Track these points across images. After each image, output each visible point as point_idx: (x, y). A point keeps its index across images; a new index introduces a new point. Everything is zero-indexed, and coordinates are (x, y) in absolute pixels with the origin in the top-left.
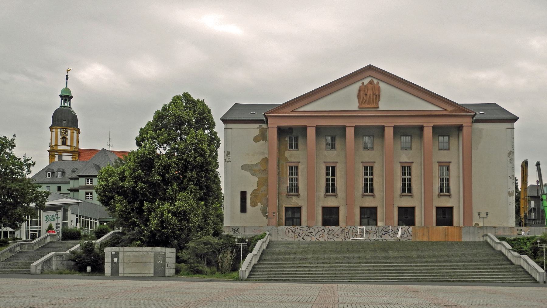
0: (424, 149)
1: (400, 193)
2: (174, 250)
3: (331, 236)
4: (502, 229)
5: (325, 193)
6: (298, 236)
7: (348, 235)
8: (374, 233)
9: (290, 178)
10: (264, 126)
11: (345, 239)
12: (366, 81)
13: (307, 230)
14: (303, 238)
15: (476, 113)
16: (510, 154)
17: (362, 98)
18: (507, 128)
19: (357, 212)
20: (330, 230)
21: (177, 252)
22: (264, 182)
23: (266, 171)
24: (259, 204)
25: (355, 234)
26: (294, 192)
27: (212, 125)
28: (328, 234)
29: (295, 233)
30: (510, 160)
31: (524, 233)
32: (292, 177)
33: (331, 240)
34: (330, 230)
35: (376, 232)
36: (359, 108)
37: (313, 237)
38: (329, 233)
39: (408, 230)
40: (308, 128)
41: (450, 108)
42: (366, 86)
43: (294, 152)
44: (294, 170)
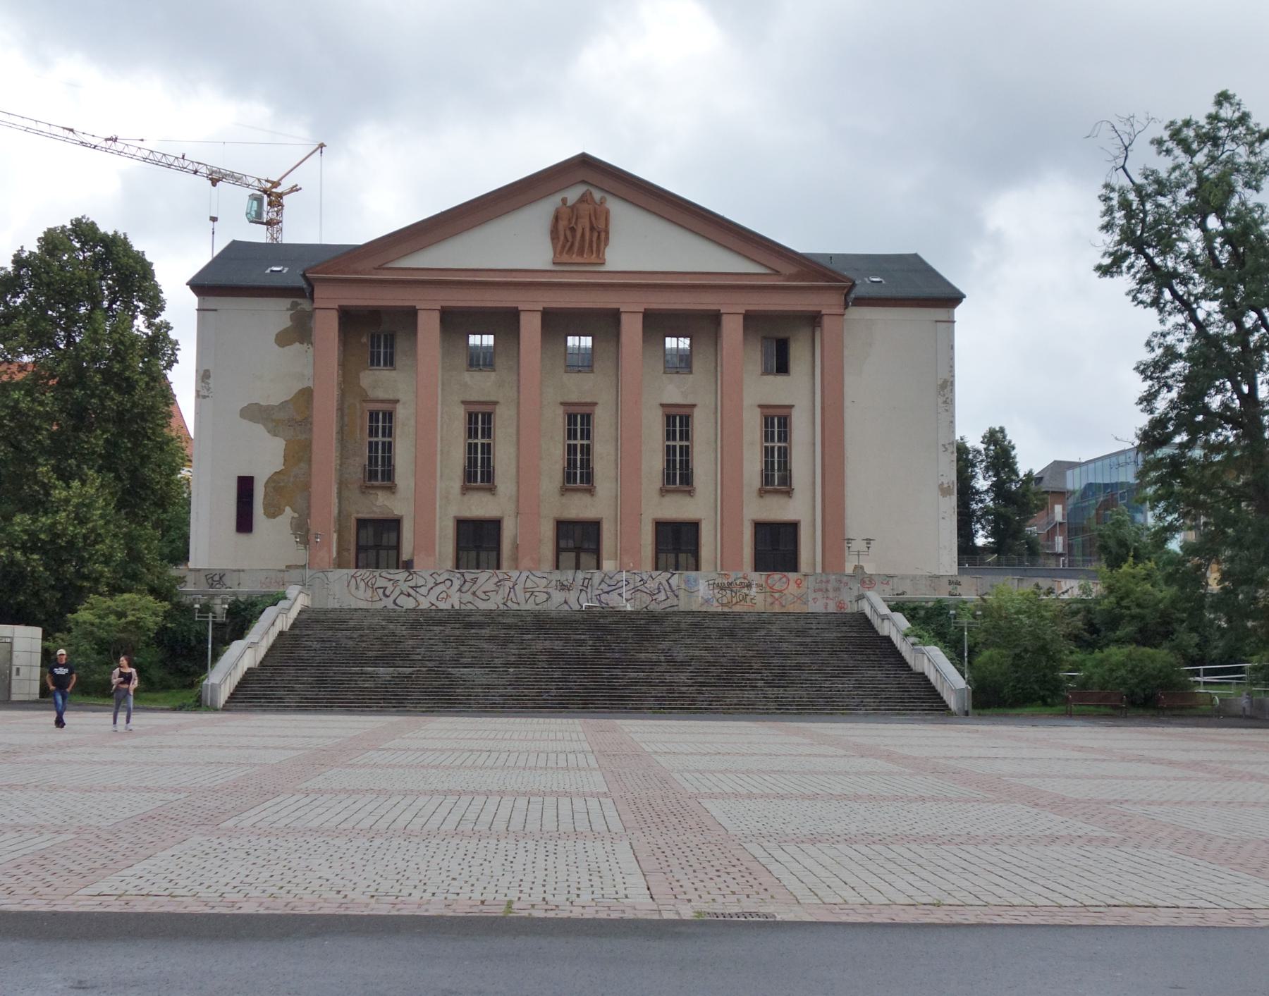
0: (722, 373)
1: (661, 486)
2: (37, 632)
3: (468, 597)
4: (908, 581)
5: (464, 482)
6: (383, 597)
7: (512, 594)
8: (581, 590)
9: (370, 443)
10: (305, 304)
11: (504, 604)
12: (573, 195)
13: (405, 581)
14: (394, 602)
15: (854, 282)
16: (946, 388)
17: (562, 238)
18: (937, 321)
19: (547, 531)
20: (465, 581)
21: (45, 637)
22: (299, 453)
23: (305, 423)
24: (288, 509)
25: (533, 592)
26: (383, 480)
27: (155, 305)
28: (460, 590)
29: (375, 589)
30: (945, 402)
31: (971, 591)
32: (376, 439)
33: (470, 607)
34: (465, 581)
35: (587, 587)
36: (554, 263)
37: (421, 599)
38: (464, 589)
39: (669, 584)
40: (420, 313)
41: (788, 269)
42: (573, 207)
43: (384, 374)
44: (384, 422)
